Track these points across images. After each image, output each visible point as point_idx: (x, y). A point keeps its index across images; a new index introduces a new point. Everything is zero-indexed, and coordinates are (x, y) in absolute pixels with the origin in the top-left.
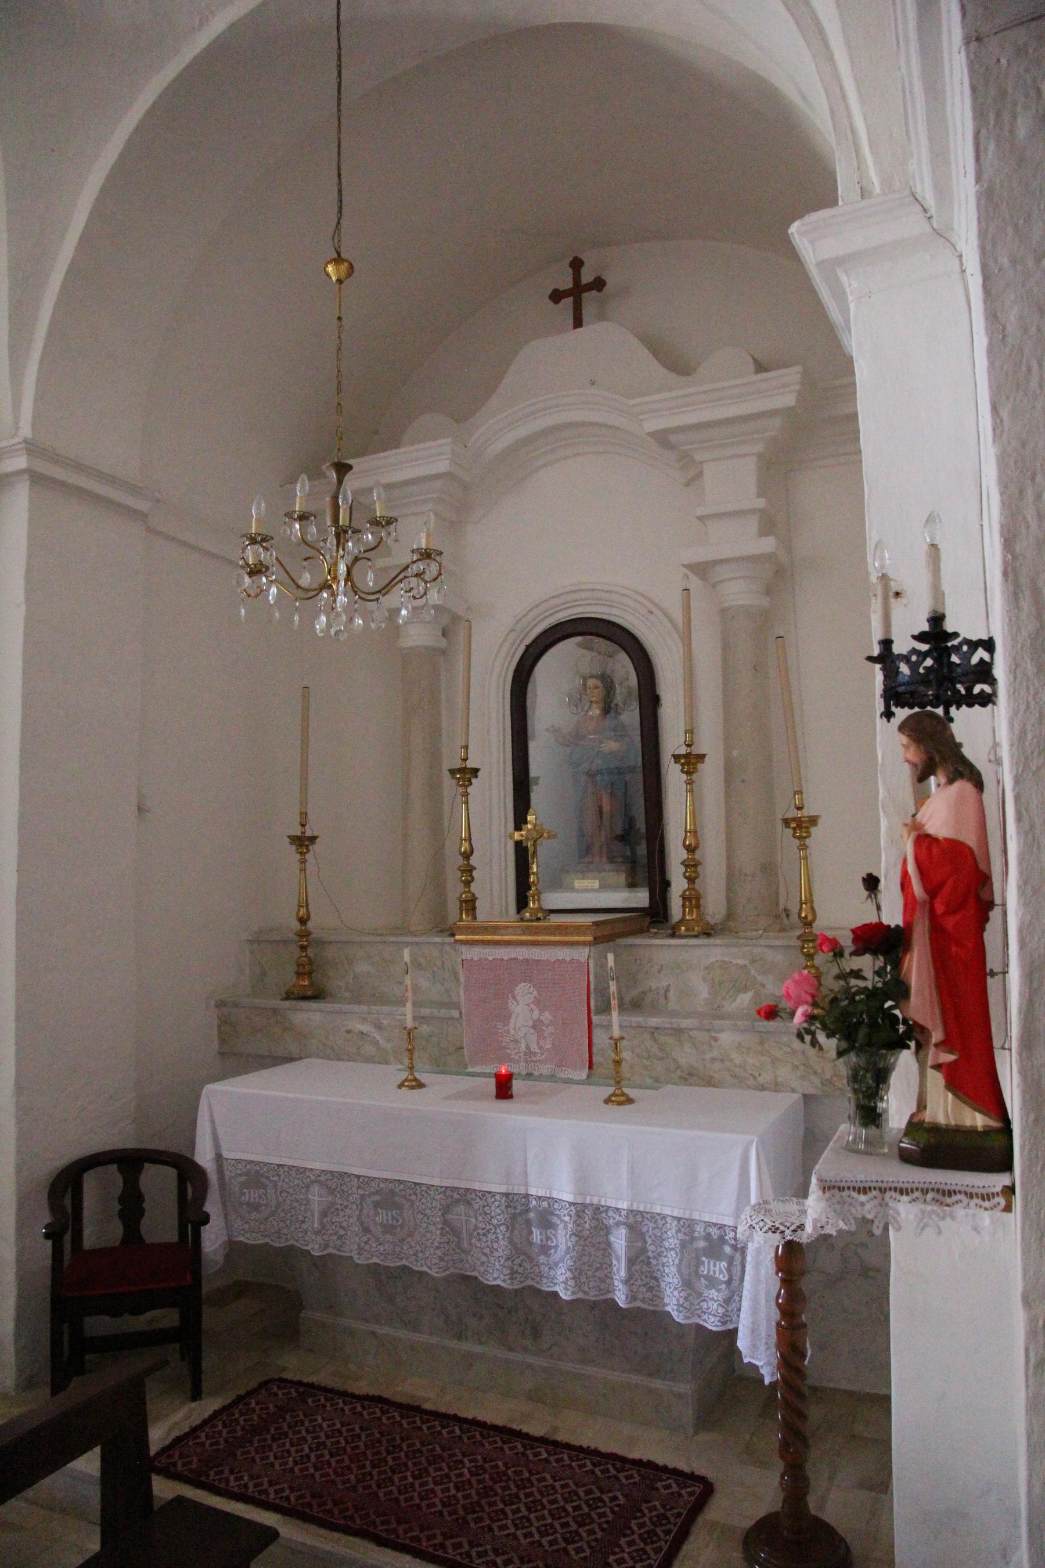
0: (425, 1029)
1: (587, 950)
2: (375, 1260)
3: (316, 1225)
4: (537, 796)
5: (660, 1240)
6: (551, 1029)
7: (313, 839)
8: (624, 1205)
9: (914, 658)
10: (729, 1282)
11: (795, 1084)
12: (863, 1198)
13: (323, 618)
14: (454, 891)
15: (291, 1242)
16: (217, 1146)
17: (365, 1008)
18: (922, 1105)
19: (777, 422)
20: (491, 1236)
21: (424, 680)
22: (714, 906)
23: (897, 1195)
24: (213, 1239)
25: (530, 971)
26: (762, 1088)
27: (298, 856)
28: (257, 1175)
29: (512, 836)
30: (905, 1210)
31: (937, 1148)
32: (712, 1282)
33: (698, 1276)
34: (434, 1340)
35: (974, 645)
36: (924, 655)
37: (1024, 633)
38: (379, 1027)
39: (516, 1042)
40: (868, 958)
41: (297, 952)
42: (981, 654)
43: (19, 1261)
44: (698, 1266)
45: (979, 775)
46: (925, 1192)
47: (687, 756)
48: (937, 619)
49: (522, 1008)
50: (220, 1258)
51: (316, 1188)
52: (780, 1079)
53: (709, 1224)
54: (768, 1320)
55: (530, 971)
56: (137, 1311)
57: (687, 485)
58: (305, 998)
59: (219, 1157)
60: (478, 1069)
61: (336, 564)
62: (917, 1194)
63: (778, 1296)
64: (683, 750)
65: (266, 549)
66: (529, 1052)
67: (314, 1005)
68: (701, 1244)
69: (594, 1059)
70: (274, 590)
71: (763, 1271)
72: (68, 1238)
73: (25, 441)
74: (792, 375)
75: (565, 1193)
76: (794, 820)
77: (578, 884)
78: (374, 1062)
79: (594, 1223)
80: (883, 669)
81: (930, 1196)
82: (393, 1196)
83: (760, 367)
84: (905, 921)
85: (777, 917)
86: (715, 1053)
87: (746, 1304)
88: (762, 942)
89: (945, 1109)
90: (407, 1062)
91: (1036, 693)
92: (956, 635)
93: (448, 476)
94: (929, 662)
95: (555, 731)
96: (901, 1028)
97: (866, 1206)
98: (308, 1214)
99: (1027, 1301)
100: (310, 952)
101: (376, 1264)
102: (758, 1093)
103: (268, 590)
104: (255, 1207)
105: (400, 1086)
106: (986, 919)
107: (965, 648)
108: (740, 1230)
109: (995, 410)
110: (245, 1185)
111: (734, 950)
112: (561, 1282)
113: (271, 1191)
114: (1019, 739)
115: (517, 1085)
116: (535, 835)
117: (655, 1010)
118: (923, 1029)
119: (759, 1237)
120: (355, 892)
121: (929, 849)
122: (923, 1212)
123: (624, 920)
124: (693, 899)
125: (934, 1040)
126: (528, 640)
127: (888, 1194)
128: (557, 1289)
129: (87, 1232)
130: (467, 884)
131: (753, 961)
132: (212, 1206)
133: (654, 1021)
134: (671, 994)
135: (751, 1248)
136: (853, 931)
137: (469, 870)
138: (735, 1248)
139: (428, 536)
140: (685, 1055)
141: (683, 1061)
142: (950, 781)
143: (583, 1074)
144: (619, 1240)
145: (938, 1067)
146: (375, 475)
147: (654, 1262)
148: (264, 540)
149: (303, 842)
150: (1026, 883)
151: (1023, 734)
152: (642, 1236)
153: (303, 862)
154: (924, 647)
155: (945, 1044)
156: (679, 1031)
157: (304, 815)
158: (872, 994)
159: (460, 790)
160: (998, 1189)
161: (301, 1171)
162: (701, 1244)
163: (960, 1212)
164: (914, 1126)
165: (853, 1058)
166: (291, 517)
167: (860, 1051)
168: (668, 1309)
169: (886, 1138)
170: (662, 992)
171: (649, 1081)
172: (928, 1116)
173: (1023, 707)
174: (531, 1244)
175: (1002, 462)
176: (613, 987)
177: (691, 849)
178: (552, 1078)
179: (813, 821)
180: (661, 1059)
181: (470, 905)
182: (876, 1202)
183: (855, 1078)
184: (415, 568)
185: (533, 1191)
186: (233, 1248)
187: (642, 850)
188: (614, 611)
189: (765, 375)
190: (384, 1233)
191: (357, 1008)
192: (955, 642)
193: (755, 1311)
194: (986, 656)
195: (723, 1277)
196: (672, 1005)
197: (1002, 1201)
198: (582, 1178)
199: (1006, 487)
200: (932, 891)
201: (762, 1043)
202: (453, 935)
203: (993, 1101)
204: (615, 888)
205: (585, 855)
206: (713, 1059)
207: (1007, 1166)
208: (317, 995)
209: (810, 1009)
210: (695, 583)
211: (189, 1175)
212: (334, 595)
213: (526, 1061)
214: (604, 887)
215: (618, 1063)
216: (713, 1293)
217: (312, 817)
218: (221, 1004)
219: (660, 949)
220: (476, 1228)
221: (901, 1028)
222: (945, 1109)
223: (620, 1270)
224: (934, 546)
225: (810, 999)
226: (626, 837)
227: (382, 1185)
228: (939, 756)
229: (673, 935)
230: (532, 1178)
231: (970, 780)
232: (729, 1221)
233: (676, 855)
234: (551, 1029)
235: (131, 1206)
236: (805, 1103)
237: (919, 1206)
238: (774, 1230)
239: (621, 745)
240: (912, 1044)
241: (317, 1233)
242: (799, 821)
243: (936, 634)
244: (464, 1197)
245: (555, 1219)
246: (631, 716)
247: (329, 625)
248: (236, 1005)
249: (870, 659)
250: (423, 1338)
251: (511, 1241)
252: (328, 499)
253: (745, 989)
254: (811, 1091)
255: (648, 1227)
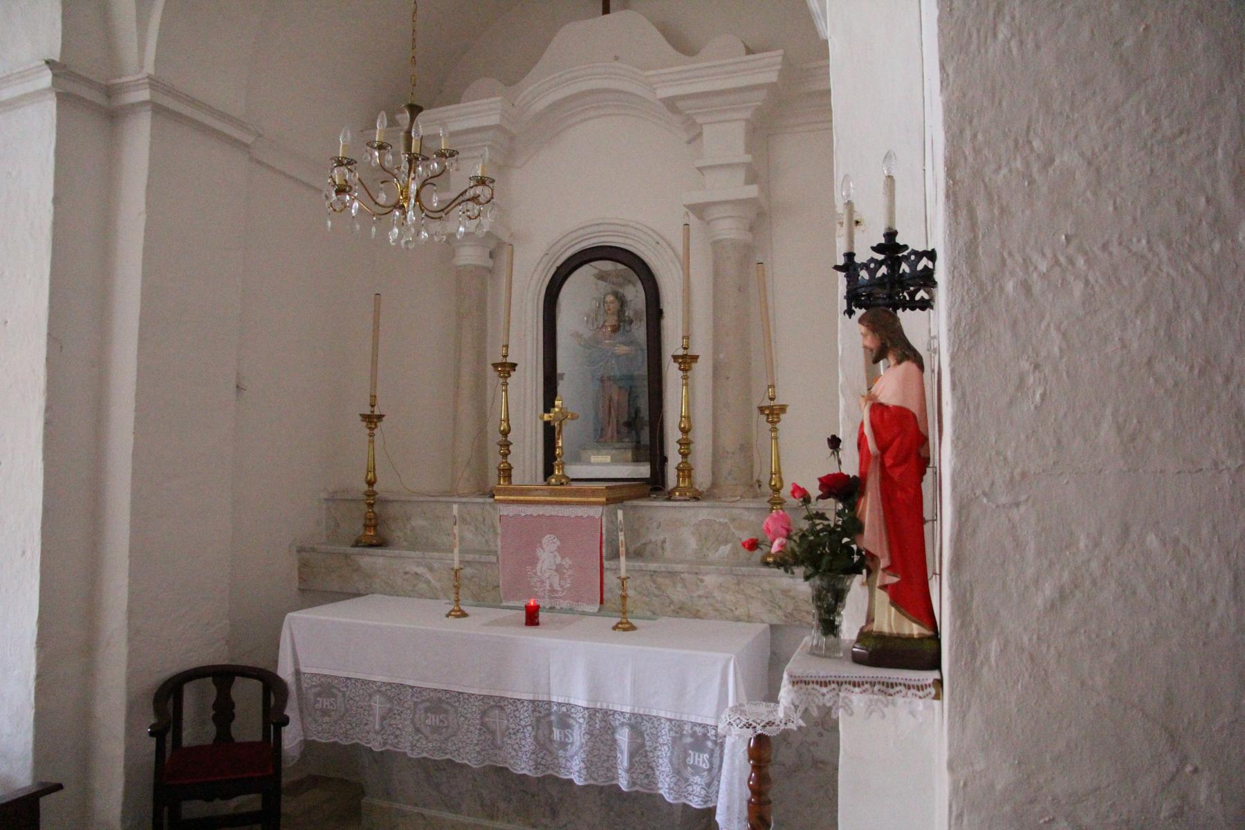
0: (468, 571)
1: (600, 509)
2: (425, 755)
3: (377, 727)
4: (562, 388)
5: (656, 737)
6: (570, 572)
7: (380, 417)
8: (627, 709)
9: (872, 266)
10: (710, 770)
11: (764, 617)
12: (824, 690)
13: (396, 230)
14: (494, 460)
15: (357, 741)
16: (296, 662)
17: (419, 554)
18: (870, 619)
19: (762, 94)
20: (520, 735)
21: (474, 292)
22: (702, 478)
23: (851, 687)
24: (291, 738)
25: (553, 525)
26: (738, 619)
27: (368, 431)
28: (328, 687)
29: (542, 418)
30: (858, 699)
31: (882, 652)
32: (696, 770)
33: (686, 765)
34: (471, 820)
35: (920, 255)
36: (880, 264)
37: (961, 242)
38: (431, 569)
39: (542, 582)
40: (831, 501)
41: (364, 507)
42: (924, 262)
43: (127, 758)
44: (685, 758)
45: (921, 358)
46: (873, 684)
47: (683, 357)
48: (891, 235)
49: (548, 554)
50: (296, 754)
51: (377, 697)
52: (752, 613)
53: (695, 724)
54: (741, 800)
55: (553, 525)
56: (228, 796)
57: (689, 142)
58: (371, 546)
59: (298, 673)
60: (511, 604)
61: (407, 187)
62: (867, 686)
63: (749, 779)
64: (681, 352)
65: (350, 171)
66: (553, 591)
67: (379, 551)
68: (689, 740)
69: (605, 596)
70: (356, 204)
71: (737, 762)
72: (169, 737)
73: (149, 77)
74: (776, 57)
75: (580, 699)
76: (768, 407)
77: (593, 459)
78: (426, 597)
79: (603, 724)
80: (847, 276)
81: (876, 688)
82: (440, 703)
83: (749, 51)
84: (861, 472)
85: (752, 486)
86: (701, 592)
87: (723, 786)
88: (739, 505)
89: (889, 620)
90: (453, 597)
91: (969, 289)
92: (906, 247)
93: (498, 127)
94: (883, 270)
95: (577, 335)
96: (856, 558)
97: (825, 696)
98: (371, 718)
99: (951, 767)
100: (376, 509)
101: (424, 758)
102: (734, 624)
103: (351, 207)
104: (325, 712)
105: (447, 616)
106: (924, 473)
107: (913, 257)
108: (720, 726)
109: (943, 67)
110: (319, 694)
111: (716, 511)
112: (575, 772)
113: (340, 699)
114: (954, 328)
115: (542, 616)
116: (560, 416)
117: (654, 557)
118: (873, 557)
119: (736, 730)
120: (413, 463)
121: (882, 414)
122: (871, 701)
123: (629, 486)
124: (686, 471)
125: (882, 566)
126: (559, 263)
127: (844, 686)
128: (572, 777)
129: (185, 734)
130: (505, 456)
131: (733, 520)
132: (291, 711)
133: (652, 566)
134: (667, 545)
135: (729, 741)
136: (820, 479)
137: (507, 445)
138: (715, 743)
139: (483, 166)
140: (678, 594)
141: (674, 597)
142: (899, 362)
143: (595, 608)
144: (623, 737)
145: (884, 587)
146: (436, 126)
147: (651, 755)
148: (349, 163)
149: (372, 420)
150: (958, 439)
151: (957, 324)
152: (641, 734)
153: (372, 435)
154: (880, 257)
155: (890, 569)
156: (672, 574)
157: (374, 397)
158: (831, 531)
159: (501, 380)
160: (930, 681)
161: (364, 682)
162: (689, 740)
163: (900, 700)
164: (864, 636)
165: (817, 581)
166: (372, 147)
167: (822, 576)
168: (661, 792)
169: (842, 645)
170: (659, 543)
171: (649, 614)
172: (875, 627)
173: (958, 301)
174: (551, 741)
175: (948, 110)
176: (621, 537)
177: (685, 431)
178: (571, 611)
179: (783, 409)
180: (657, 596)
181: (507, 473)
182: (834, 693)
183: (818, 597)
184: (471, 193)
185: (554, 699)
186: (309, 746)
187: (645, 437)
188: (628, 241)
189: (751, 57)
190: (433, 733)
191: (413, 554)
192: (905, 253)
193: (730, 792)
194: (930, 265)
195: (706, 766)
196: (668, 554)
197: (933, 691)
198: (595, 688)
199: (949, 127)
200: (883, 447)
201: (738, 584)
202: (493, 496)
203: (927, 616)
204: (625, 462)
205: (600, 439)
206: (700, 597)
207: (936, 664)
208: (381, 543)
209: (784, 541)
210: (693, 220)
211: (272, 686)
212: (405, 213)
213: (551, 598)
214: (615, 461)
215: (624, 598)
216: (697, 779)
217: (379, 401)
218: (299, 551)
219: (658, 510)
220: (508, 728)
221: (856, 558)
222: (889, 620)
223: (623, 761)
224: (890, 177)
225: (785, 533)
226: (632, 424)
227: (432, 694)
228: (890, 344)
229: (669, 499)
230: (553, 691)
231: (914, 361)
232: (711, 722)
233: (673, 435)
234: (570, 572)
235: (224, 711)
236: (772, 633)
237: (866, 697)
238: (748, 726)
239: (627, 351)
240: (864, 571)
241: (377, 733)
242: (771, 408)
243: (890, 247)
244: (499, 703)
245: (572, 721)
246: (640, 331)
247: (400, 236)
248: (313, 550)
249: (837, 268)
250: (461, 818)
251: (536, 738)
252: (402, 134)
253: (726, 542)
254: (775, 621)
255: (646, 726)
